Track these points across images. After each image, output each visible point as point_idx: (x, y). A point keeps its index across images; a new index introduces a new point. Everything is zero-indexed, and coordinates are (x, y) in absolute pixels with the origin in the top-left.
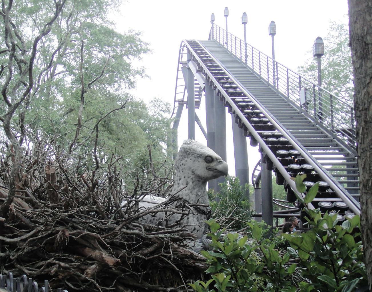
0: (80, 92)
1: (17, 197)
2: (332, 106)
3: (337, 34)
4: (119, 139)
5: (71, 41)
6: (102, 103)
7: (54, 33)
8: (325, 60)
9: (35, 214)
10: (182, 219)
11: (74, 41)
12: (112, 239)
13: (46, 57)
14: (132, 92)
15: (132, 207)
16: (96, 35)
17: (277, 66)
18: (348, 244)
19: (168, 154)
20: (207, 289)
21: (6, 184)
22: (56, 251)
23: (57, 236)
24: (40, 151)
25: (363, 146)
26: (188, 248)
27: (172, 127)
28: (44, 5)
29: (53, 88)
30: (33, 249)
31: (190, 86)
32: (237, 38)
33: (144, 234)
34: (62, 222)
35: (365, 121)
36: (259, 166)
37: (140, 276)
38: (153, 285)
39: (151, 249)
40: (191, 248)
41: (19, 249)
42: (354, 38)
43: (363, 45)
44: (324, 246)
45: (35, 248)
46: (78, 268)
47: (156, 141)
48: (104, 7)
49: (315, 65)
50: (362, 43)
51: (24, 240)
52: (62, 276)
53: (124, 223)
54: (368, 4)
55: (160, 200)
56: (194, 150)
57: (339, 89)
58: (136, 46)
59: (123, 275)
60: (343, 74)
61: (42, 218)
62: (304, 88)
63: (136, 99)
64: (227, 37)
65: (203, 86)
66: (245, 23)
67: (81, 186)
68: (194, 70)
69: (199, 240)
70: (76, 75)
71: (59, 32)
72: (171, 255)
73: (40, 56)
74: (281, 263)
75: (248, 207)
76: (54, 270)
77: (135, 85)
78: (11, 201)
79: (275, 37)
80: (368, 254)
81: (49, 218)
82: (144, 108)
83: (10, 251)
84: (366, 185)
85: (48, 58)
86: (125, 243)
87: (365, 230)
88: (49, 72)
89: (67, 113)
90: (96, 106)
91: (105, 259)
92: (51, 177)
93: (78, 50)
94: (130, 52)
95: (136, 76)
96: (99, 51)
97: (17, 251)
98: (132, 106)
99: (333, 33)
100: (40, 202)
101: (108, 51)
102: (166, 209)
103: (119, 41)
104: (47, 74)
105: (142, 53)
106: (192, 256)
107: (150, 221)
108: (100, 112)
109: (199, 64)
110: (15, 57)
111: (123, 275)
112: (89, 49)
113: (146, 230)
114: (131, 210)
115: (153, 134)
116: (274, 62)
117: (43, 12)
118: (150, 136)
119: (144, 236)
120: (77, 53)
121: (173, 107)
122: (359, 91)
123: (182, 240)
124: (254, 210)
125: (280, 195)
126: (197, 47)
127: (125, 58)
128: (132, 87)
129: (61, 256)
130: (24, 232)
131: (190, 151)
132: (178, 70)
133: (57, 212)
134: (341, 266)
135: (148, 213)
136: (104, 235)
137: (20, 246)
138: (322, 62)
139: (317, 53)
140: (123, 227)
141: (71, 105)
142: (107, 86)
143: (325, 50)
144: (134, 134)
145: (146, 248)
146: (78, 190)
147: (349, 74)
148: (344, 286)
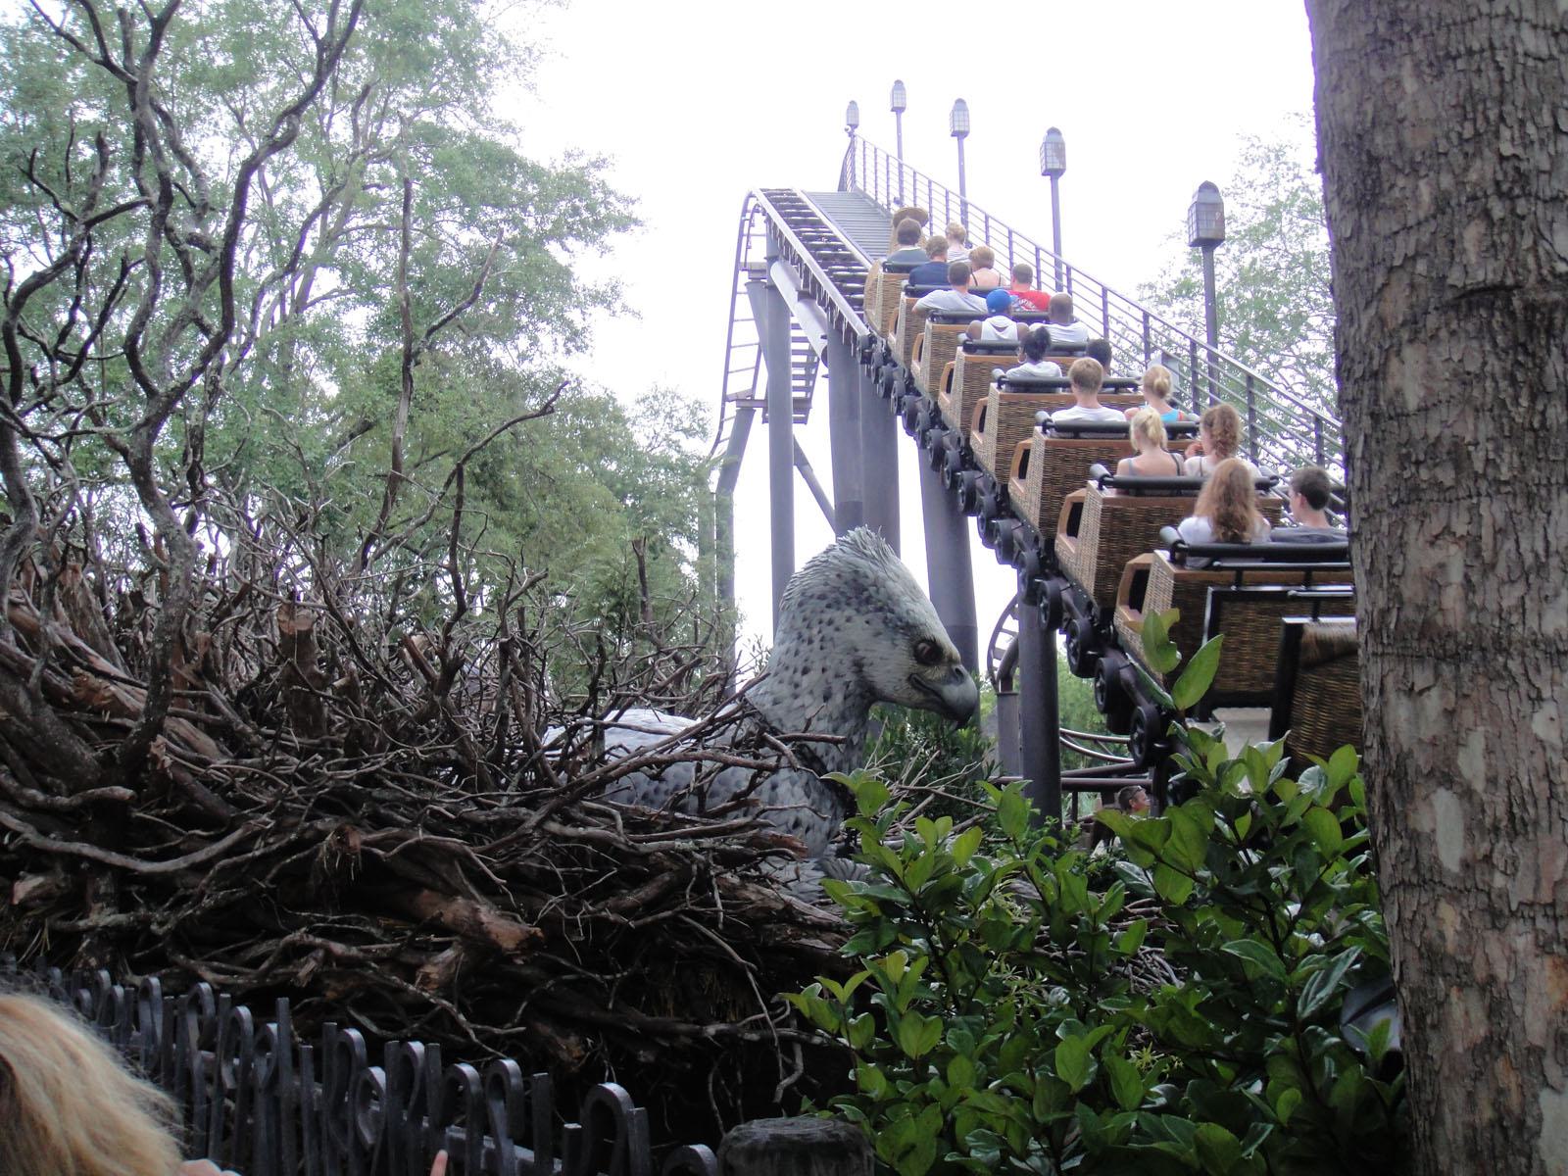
0: (399, 364)
1: (177, 715)
2: (1252, 411)
3: (1265, 177)
4: (532, 527)
5: (365, 187)
6: (474, 403)
7: (305, 158)
8: (1227, 263)
9: (241, 773)
10: (753, 786)
11: (379, 187)
12: (511, 858)
13: (278, 242)
14: (575, 366)
15: (580, 750)
16: (451, 166)
17: (1069, 280)
18: (1320, 843)
19: (702, 578)
20: (847, 1005)
21: (136, 670)
22: (315, 906)
23: (317, 852)
24: (257, 553)
25: (1367, 498)
26: (775, 886)
27: (713, 488)
28: (272, 60)
29: (303, 349)
30: (233, 898)
31: (775, 345)
32: (934, 186)
33: (622, 839)
34: (339, 802)
35: (1372, 415)
36: (1010, 617)
37: (610, 987)
38: (657, 1018)
39: (647, 892)
40: (785, 885)
41: (185, 899)
42: (1333, 141)
43: (1360, 162)
44: (1241, 853)
45: (241, 893)
46: (391, 960)
47: (661, 533)
48: (480, 73)
49: (1193, 280)
50: (1359, 154)
51: (200, 868)
52: (335, 990)
53: (554, 801)
54: (1376, 29)
55: (679, 724)
56: (890, 598)
57: (1274, 358)
58: (591, 208)
59: (551, 982)
60: (1284, 309)
61: (266, 787)
62: (1159, 353)
63: (592, 389)
64: (901, 182)
65: (819, 345)
66: (960, 135)
67: (406, 675)
68: (788, 291)
69: (812, 863)
70: (383, 304)
71: (323, 152)
72: (717, 912)
73: (254, 239)
74: (1095, 918)
75: (978, 753)
76: (307, 967)
77: (587, 341)
78: (154, 729)
79: (1061, 181)
80: (1386, 859)
81: (289, 789)
82: (618, 418)
83: (152, 905)
84: (1380, 629)
85: (284, 243)
86: (558, 871)
87: (1379, 781)
88: (289, 294)
89: (352, 436)
90: (454, 412)
91: (490, 927)
92: (297, 644)
93: (391, 219)
94: (570, 229)
95: (591, 309)
96: (462, 224)
97: (177, 906)
98: (576, 415)
99: (1253, 173)
100: (257, 732)
101: (495, 223)
102: (700, 751)
103: (532, 189)
104: (282, 299)
105: (612, 231)
106: (788, 914)
107: (645, 797)
108: (466, 434)
109: (807, 271)
110: (169, 230)
111: (551, 982)
112: (428, 214)
113: (632, 825)
114: (579, 758)
115: (649, 512)
116: (1058, 264)
117: (269, 85)
118: (637, 520)
119: (622, 847)
120: (387, 228)
121: (719, 419)
122: (1351, 314)
123: (754, 858)
124: (997, 762)
125: (1083, 717)
126: (798, 214)
127: (553, 247)
128: (578, 348)
129: (334, 921)
130: (200, 836)
131: (877, 592)
132: (735, 293)
133: (319, 766)
134: (1297, 918)
135: (636, 768)
136: (483, 844)
137: (186, 888)
138: (1218, 269)
139: (1203, 235)
140: (548, 817)
141: (364, 407)
142: (489, 342)
143: (1228, 231)
144: (585, 509)
145: (630, 891)
146: (392, 691)
147: (1305, 309)
148: (1311, 973)
